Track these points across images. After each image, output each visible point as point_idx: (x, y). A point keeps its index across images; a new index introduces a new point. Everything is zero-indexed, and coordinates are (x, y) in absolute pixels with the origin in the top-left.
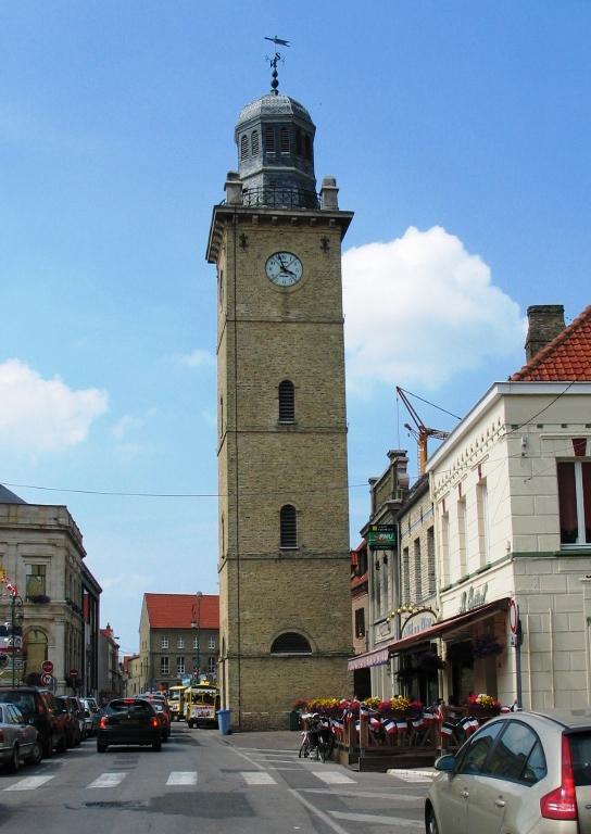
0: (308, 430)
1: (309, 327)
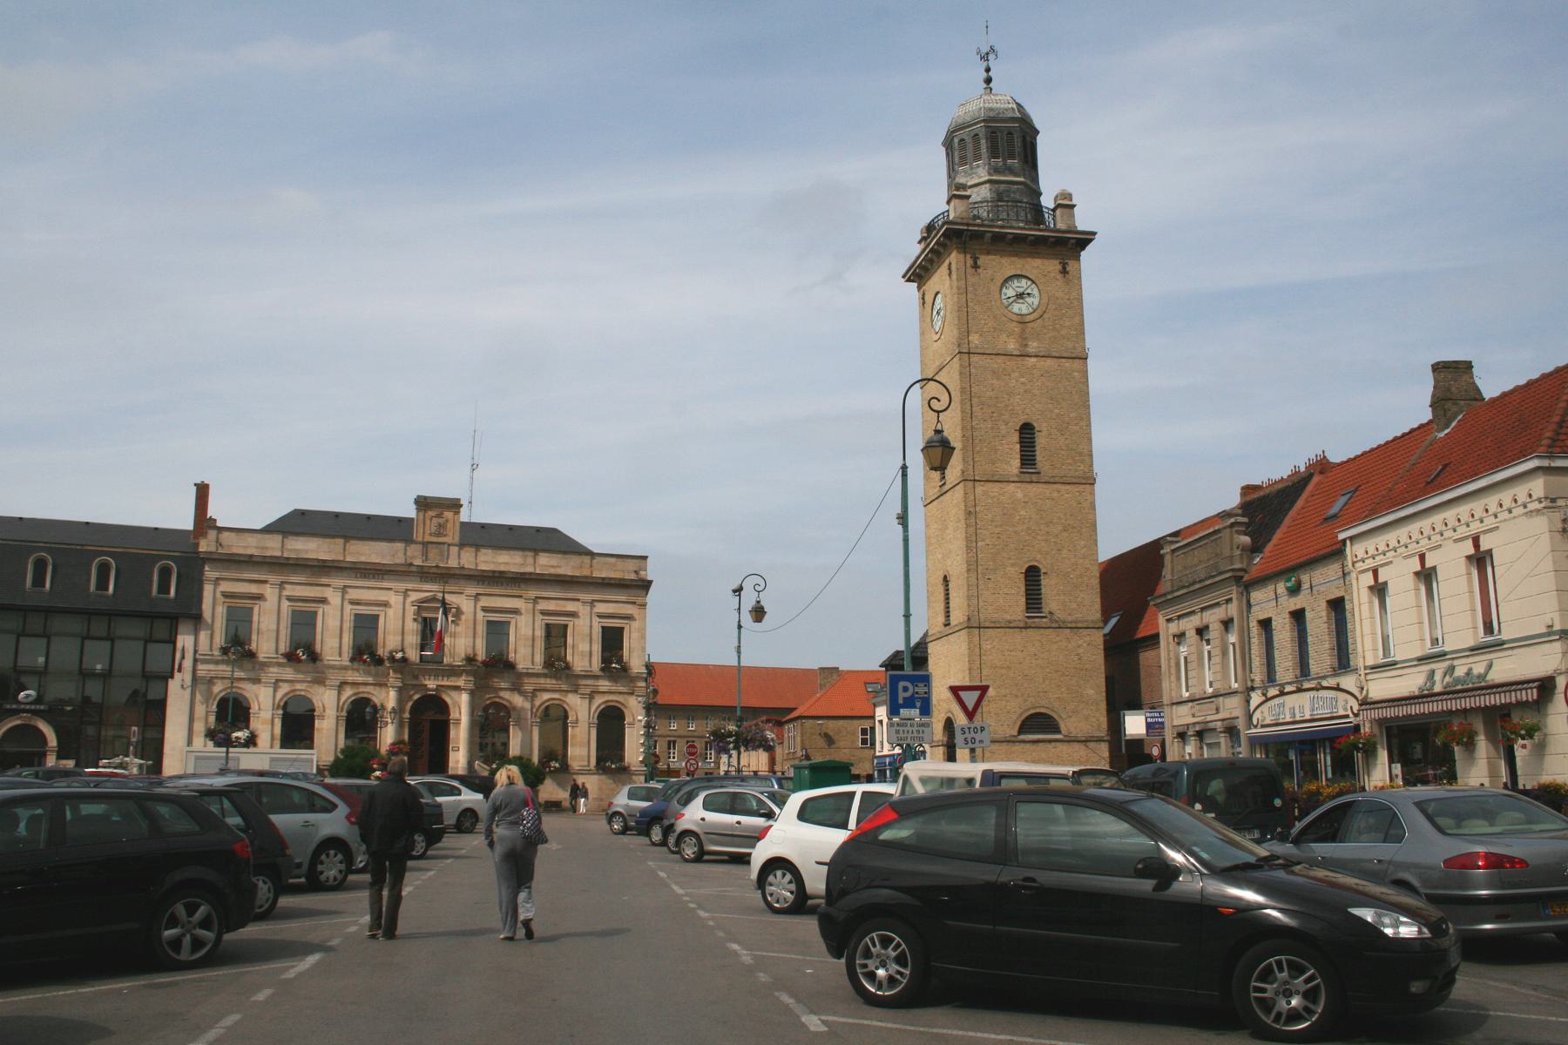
0: (1052, 480)
1: (1049, 362)
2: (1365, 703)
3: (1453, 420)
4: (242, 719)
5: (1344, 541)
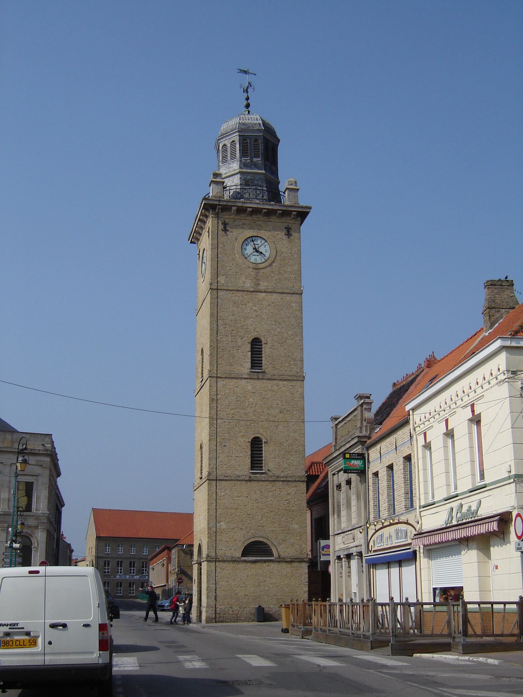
0: (273, 378)
1: (275, 295)
2: (420, 534)
3: (496, 323)
5: (409, 411)
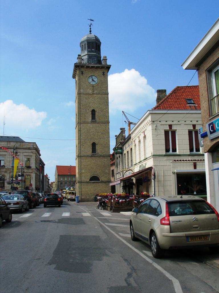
1: (99, 95)
4: (3, 178)
